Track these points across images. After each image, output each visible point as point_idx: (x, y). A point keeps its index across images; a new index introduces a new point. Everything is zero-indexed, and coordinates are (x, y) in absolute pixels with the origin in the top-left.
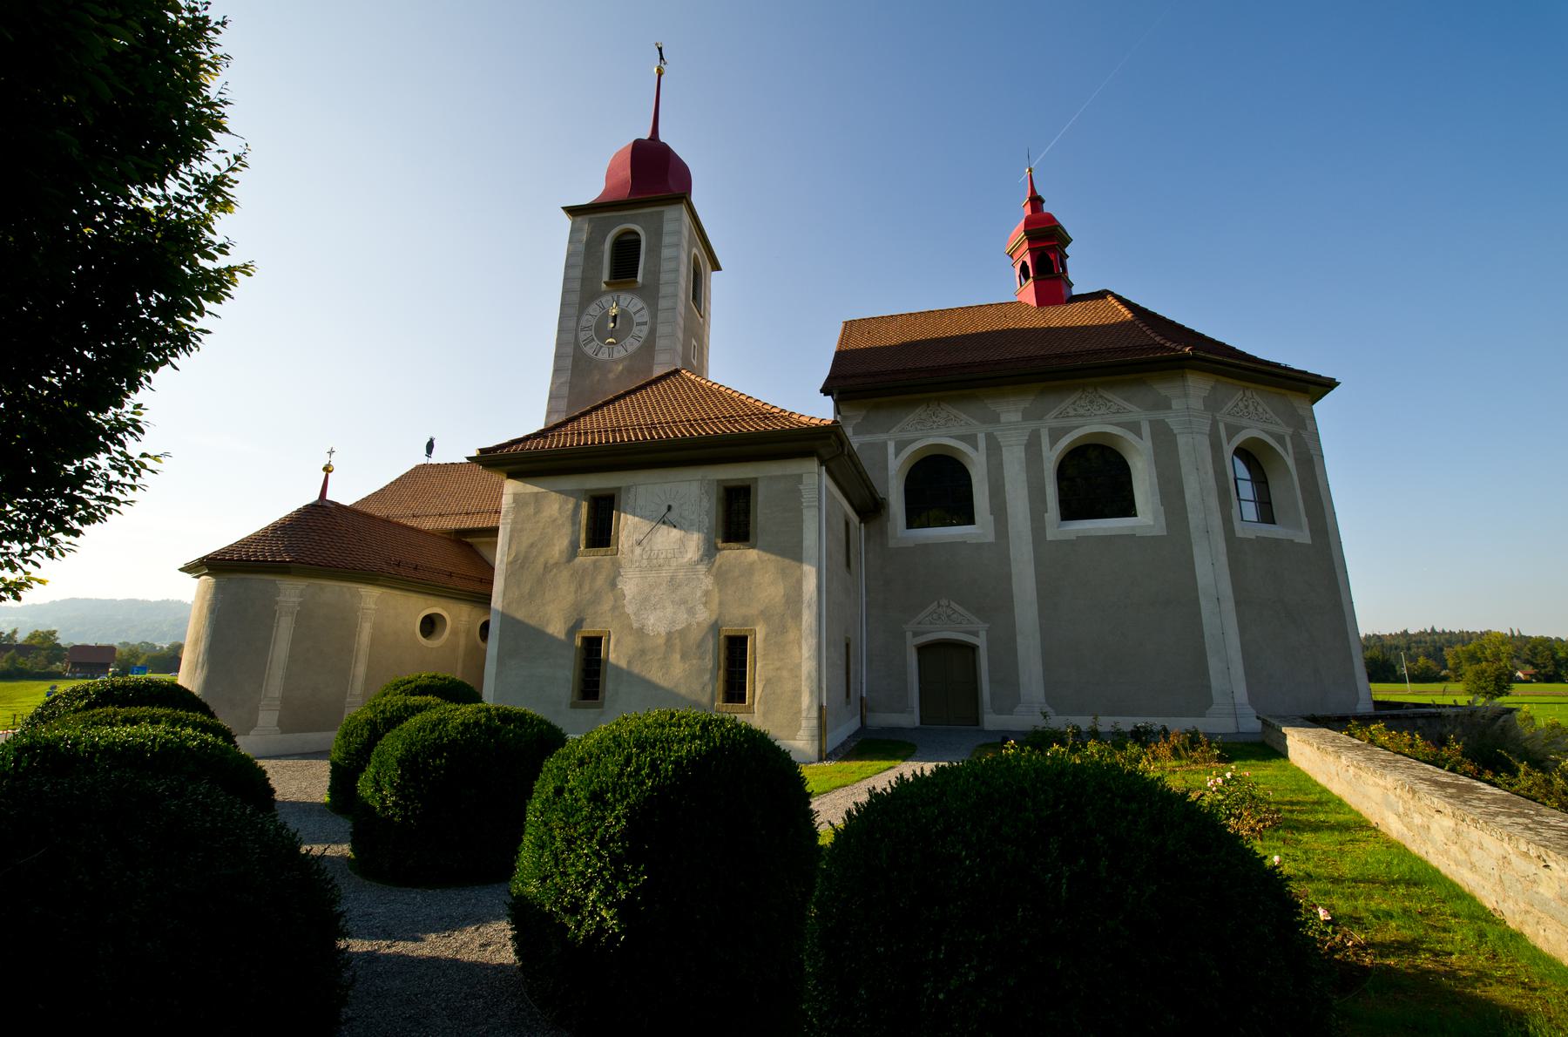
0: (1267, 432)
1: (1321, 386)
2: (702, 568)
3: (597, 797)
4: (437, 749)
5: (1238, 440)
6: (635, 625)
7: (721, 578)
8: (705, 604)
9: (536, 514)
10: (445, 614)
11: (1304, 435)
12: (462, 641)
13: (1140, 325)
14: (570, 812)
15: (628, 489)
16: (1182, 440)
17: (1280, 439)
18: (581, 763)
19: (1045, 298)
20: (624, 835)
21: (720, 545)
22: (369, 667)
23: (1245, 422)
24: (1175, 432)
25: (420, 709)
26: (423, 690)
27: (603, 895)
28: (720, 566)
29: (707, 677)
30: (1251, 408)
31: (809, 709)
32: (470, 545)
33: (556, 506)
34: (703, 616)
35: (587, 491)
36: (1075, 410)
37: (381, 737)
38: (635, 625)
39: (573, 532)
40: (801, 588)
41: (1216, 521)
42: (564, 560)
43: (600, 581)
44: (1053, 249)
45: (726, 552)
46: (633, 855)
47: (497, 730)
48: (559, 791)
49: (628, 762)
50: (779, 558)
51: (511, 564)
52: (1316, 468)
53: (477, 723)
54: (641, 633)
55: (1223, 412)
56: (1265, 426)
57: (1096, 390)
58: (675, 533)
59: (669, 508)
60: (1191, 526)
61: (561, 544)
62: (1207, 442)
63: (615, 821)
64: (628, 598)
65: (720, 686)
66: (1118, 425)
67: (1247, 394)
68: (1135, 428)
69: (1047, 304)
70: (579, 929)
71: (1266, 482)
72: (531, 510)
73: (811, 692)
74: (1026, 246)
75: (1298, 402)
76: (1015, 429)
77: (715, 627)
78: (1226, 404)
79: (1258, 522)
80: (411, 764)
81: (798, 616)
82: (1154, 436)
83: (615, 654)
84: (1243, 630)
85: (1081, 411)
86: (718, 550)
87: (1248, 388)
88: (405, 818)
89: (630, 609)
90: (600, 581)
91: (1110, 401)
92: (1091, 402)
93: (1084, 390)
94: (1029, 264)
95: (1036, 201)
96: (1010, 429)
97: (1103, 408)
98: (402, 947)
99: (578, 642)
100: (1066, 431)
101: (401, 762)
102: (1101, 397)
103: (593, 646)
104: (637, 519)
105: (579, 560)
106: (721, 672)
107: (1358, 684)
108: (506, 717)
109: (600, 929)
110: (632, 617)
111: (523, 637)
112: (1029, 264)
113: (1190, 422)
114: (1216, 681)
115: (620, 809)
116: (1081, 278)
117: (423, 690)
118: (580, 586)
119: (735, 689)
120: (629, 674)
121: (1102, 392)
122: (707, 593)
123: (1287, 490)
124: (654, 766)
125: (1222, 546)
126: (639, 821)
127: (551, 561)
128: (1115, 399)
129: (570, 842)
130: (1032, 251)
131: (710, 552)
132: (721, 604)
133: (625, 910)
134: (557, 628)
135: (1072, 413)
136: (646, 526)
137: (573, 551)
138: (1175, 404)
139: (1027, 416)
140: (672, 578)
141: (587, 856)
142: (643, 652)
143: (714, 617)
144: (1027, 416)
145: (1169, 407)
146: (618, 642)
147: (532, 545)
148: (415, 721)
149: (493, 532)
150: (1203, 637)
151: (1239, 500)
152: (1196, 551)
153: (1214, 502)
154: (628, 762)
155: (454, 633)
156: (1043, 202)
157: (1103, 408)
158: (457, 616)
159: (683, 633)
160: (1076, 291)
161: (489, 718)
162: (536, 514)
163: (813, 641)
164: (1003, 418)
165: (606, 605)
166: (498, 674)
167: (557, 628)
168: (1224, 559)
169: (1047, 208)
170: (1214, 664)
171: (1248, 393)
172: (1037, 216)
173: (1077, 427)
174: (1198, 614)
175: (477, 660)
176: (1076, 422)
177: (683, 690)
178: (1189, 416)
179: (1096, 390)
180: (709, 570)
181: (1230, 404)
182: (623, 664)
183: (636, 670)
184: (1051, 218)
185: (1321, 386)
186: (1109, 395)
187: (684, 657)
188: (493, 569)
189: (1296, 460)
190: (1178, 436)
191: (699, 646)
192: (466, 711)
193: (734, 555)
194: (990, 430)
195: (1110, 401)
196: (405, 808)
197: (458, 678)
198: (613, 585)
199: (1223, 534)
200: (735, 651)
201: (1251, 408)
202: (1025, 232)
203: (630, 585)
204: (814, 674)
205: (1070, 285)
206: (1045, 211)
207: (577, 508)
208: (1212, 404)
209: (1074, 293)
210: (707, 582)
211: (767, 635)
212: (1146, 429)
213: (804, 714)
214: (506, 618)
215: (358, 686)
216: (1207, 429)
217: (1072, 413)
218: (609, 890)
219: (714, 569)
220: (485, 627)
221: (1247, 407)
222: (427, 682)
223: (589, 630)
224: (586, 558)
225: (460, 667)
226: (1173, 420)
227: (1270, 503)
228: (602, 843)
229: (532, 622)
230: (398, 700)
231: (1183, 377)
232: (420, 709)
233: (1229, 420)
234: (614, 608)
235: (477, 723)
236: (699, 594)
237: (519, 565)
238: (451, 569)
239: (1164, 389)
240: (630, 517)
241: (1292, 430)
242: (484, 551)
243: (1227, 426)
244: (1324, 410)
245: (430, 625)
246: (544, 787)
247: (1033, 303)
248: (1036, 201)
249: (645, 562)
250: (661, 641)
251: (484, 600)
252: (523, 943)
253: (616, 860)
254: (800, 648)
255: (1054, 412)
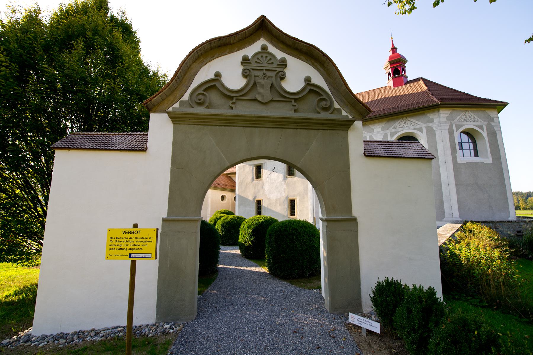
0: (474, 125)
1: (500, 106)
2: (283, 183)
3: (248, 227)
4: (227, 223)
5: (462, 129)
6: (268, 197)
7: (288, 185)
8: (284, 192)
9: (244, 171)
10: (226, 196)
11: (492, 124)
12: (230, 202)
13: (428, 92)
14: (245, 229)
15: (264, 163)
16: (437, 133)
17: (481, 127)
18: (247, 223)
19: (395, 85)
20: (252, 232)
21: (287, 177)
22: (211, 208)
23: (465, 123)
24: (435, 130)
25: (222, 217)
26: (223, 213)
27: (249, 240)
28: (287, 182)
29: (286, 210)
30: (468, 117)
31: (311, 218)
32: (230, 177)
33: (248, 169)
34: (284, 195)
35: (255, 164)
36: (399, 126)
37: (216, 222)
38: (268, 197)
39: (252, 175)
40: (308, 187)
41: (450, 158)
42: (251, 182)
43: (260, 187)
44: (400, 66)
45: (289, 178)
46: (253, 235)
47: (237, 220)
48: (243, 227)
49: (253, 222)
50: (302, 179)
51: (239, 183)
52: (497, 136)
53: (233, 219)
54: (269, 199)
55: (455, 121)
56: (475, 123)
57: (407, 118)
58: (276, 174)
59: (274, 168)
60: (439, 161)
61: (250, 178)
62: (447, 132)
63: (250, 231)
64: (266, 190)
65: (289, 212)
66: (414, 129)
67: (466, 113)
68: (420, 130)
69: (397, 86)
70: (247, 245)
71: (476, 143)
72: (243, 170)
73: (311, 214)
74: (390, 66)
75: (492, 113)
76: (379, 134)
77: (287, 198)
78: (457, 118)
79: (475, 157)
80: (223, 225)
81: (307, 194)
82: (427, 132)
83: (264, 204)
84: (458, 193)
85: (402, 126)
86: (287, 178)
87: (467, 110)
88: (223, 234)
89: (267, 194)
90: (260, 187)
91: (411, 122)
92: (405, 122)
93: (403, 119)
94: (391, 73)
95: (394, 49)
96: (377, 134)
97: (409, 124)
98: (225, 252)
99: (256, 201)
100: (396, 133)
101: (221, 225)
102: (408, 120)
103: (259, 202)
104: (267, 171)
105: (254, 182)
106: (289, 209)
107: (510, 211)
108: (238, 218)
109: (249, 245)
110: (268, 196)
111: (243, 200)
112: (391, 73)
113: (441, 126)
114: (447, 210)
115: (251, 229)
116: (411, 73)
117: (223, 213)
118: (255, 188)
119: (293, 213)
120: (268, 209)
121: (409, 119)
122: (285, 189)
123: (484, 144)
124: (256, 223)
125: (451, 167)
126: (254, 230)
127: (248, 182)
128: (414, 120)
129: (245, 233)
130: (391, 68)
131: (285, 178)
132: (288, 192)
133: (252, 242)
134: (251, 198)
135: (398, 127)
136: (269, 172)
137: (253, 180)
138: (435, 120)
139: (383, 129)
140: (276, 186)
141: (247, 236)
142: (270, 204)
143: (287, 195)
144: (383, 129)
145: (433, 122)
146: (264, 202)
147: (243, 179)
148: (223, 218)
149: (235, 173)
150: (443, 196)
151: (470, 150)
152: (441, 169)
153: (449, 152)
154: (253, 222)
155: (228, 200)
156: (396, 49)
157: (409, 124)
158: (229, 195)
159: (279, 199)
160: (409, 79)
161: (235, 218)
162: (244, 171)
163: (311, 201)
164: (375, 130)
165: (261, 193)
166: (238, 209)
167: (251, 198)
168: (452, 171)
169: (399, 51)
170: (446, 205)
171: (467, 113)
172: (394, 54)
173: (400, 131)
174: (441, 189)
175: (234, 206)
176: (400, 129)
177: (280, 213)
178: (440, 124)
179: (407, 118)
180: (285, 183)
181: (458, 118)
182: (266, 206)
183: (269, 207)
184: (399, 55)
185: (500, 106)
186: (411, 120)
187: (280, 205)
188: (235, 182)
189: (488, 134)
190: (436, 131)
191: (283, 202)
192: (231, 217)
193: (291, 179)
194: (371, 135)
195: (411, 122)
196: (222, 233)
197: (230, 210)
198: (263, 188)
199: (452, 162)
200: (292, 203)
201: (468, 117)
202: (389, 62)
203: (266, 187)
204: (312, 209)
205: (407, 77)
206: (398, 52)
207: (253, 169)
208: (450, 119)
209: (408, 80)
210: (285, 186)
211: (300, 199)
212: (424, 130)
213: (310, 219)
214: (239, 196)
215: (209, 213)
216: (448, 127)
217: (398, 127)
218: (250, 239)
219: (286, 183)
220: (235, 197)
221: (466, 117)
222: (224, 211)
223: (258, 199)
224: (257, 181)
225: (230, 208)
226: (434, 126)
227: (477, 150)
228: (249, 233)
229: (245, 197)
230: (219, 215)
231: (438, 111)
232: (222, 217)
233: (458, 123)
234: (263, 193)
235: (233, 219)
236: (283, 189)
237: (241, 183)
238: (227, 184)
239: (432, 116)
240: (265, 170)
241: (487, 123)
242: (233, 178)
243: (457, 126)
244: (503, 116)
245: (223, 198)
246: (242, 226)
247: (392, 86)
248: (394, 49)
249: (269, 182)
250: (274, 201)
251: (234, 191)
252: (241, 249)
253: (251, 235)
254: (308, 202)
255: (393, 127)
